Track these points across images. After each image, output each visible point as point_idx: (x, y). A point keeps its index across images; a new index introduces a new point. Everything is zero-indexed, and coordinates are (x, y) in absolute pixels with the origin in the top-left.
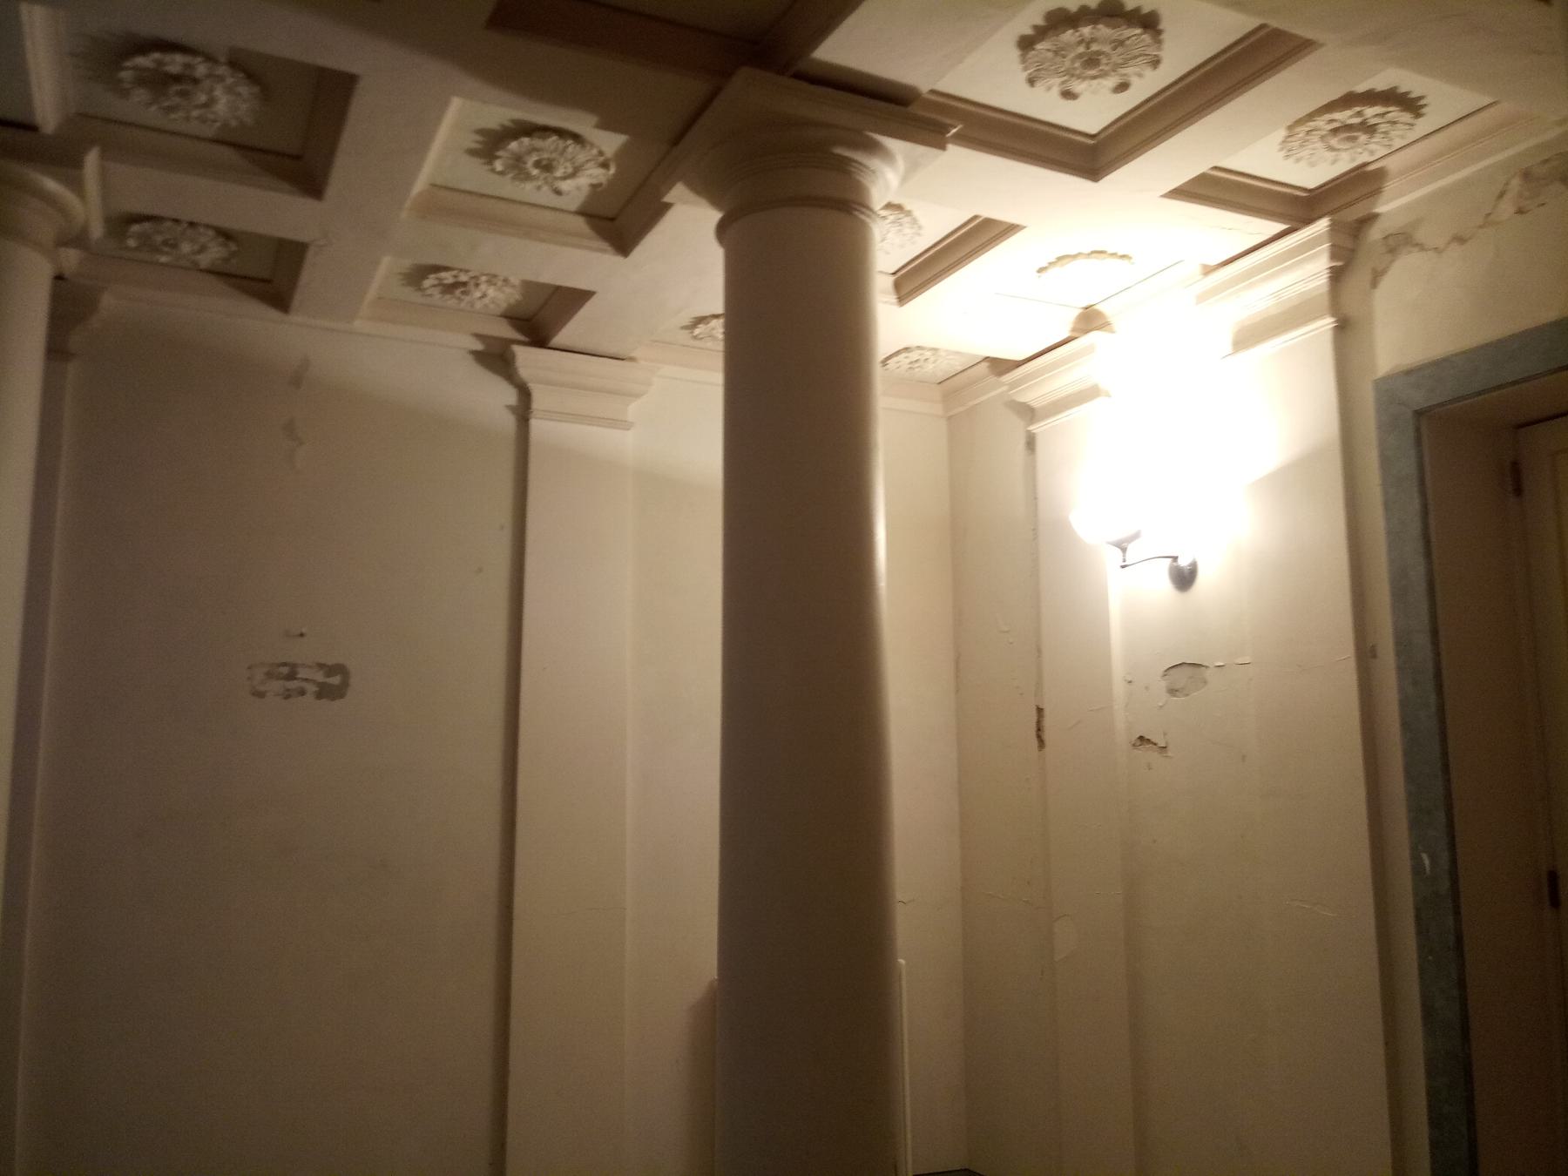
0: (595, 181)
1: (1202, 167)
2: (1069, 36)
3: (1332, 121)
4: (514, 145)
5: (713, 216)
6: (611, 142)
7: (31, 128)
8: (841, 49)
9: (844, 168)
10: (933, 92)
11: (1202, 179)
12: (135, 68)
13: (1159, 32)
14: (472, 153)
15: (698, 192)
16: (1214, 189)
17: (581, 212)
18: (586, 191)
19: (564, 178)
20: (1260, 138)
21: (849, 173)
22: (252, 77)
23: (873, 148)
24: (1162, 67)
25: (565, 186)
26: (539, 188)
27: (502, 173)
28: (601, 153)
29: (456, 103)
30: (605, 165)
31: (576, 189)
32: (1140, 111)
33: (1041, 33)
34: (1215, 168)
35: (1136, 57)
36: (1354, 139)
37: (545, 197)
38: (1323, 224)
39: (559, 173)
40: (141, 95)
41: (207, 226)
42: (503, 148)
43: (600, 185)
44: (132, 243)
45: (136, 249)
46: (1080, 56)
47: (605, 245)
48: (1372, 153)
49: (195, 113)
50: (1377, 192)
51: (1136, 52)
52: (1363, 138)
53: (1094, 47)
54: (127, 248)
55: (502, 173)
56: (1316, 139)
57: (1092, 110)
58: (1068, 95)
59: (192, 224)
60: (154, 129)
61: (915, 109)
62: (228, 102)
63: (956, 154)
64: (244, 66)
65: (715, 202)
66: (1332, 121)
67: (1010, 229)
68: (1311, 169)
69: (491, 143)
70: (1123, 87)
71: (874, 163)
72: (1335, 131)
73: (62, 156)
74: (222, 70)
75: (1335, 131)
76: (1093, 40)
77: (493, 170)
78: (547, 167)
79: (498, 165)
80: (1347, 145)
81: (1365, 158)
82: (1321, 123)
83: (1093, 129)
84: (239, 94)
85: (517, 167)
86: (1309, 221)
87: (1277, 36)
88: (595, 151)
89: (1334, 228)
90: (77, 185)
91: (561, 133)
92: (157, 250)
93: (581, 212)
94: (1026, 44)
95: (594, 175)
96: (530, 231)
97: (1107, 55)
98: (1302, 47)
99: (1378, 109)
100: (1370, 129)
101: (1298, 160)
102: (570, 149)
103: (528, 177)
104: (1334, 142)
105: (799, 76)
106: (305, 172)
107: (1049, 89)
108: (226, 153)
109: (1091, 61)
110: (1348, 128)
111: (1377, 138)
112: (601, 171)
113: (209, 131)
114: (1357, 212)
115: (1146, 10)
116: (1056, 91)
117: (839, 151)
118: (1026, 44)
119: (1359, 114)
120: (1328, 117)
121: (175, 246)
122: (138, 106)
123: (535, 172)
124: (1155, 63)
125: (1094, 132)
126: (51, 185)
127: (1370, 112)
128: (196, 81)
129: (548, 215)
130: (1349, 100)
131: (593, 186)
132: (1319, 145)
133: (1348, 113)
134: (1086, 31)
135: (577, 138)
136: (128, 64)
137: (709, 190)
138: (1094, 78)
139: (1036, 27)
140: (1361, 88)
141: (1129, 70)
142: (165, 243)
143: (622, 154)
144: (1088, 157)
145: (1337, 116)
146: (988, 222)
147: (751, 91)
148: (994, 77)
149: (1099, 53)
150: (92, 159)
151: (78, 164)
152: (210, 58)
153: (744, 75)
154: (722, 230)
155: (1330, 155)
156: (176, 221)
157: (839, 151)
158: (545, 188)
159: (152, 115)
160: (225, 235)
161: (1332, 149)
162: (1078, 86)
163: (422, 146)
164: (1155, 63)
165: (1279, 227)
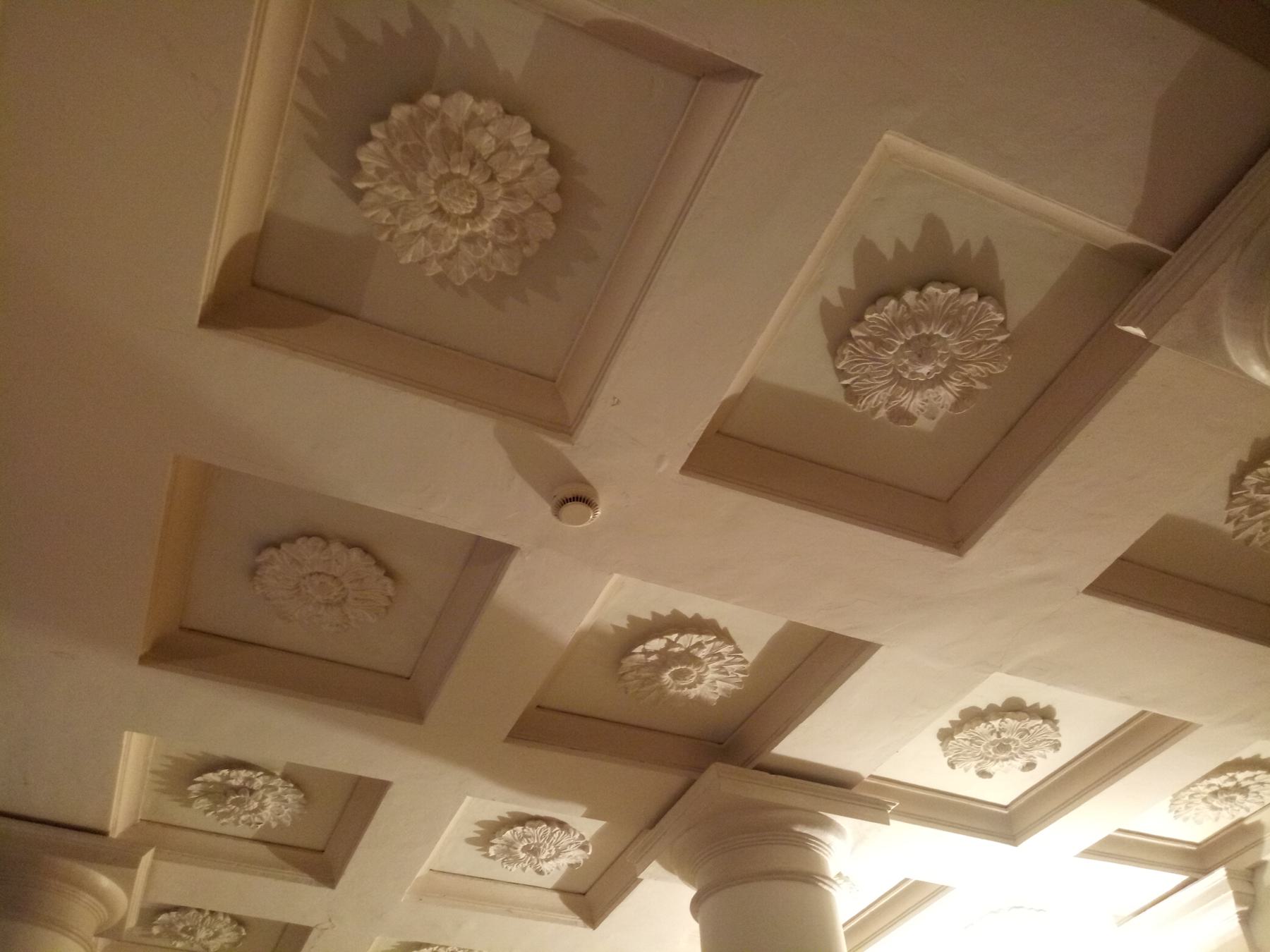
0: (573, 861)
1: (1109, 830)
2: (982, 728)
3: (1209, 786)
4: (508, 833)
5: (690, 892)
6: (590, 827)
7: (103, 833)
8: (799, 745)
9: (803, 842)
10: (872, 776)
11: (1109, 840)
12: (204, 782)
13: (1056, 722)
14: (470, 841)
15: (671, 871)
16: (1122, 848)
17: (555, 889)
18: (564, 869)
19: (547, 860)
20: (1160, 802)
21: (808, 848)
22: (298, 786)
23: (827, 825)
24: (1061, 749)
25: (545, 867)
26: (524, 869)
27: (494, 858)
28: (582, 837)
29: (468, 798)
30: (584, 847)
31: (555, 869)
32: (1045, 785)
33: (958, 726)
34: (1120, 830)
35: (1038, 743)
36: (1233, 799)
37: (529, 876)
38: (1220, 874)
39: (543, 857)
40: (204, 803)
41: (225, 915)
42: (500, 837)
43: (578, 864)
44: (156, 930)
45: (159, 936)
46: (992, 743)
47: (577, 918)
48: (1248, 810)
49: (243, 818)
50: (1259, 842)
51: (1039, 739)
52: (1239, 797)
53: (1004, 736)
54: (150, 936)
55: (494, 858)
56: (1200, 801)
57: (1005, 785)
58: (983, 774)
59: (212, 913)
60: (211, 833)
61: (856, 790)
62: (274, 807)
63: (898, 828)
64: (295, 778)
65: (689, 880)
66: (1209, 786)
67: (941, 890)
68: (1200, 825)
69: (488, 833)
70: (1030, 766)
71: (829, 838)
72: (1215, 794)
73: (122, 859)
74: (278, 782)
75: (1215, 794)
76: (1003, 730)
77: (487, 856)
78: (533, 851)
79: (492, 851)
80: (1228, 804)
81: (1243, 814)
82: (1201, 788)
83: (1005, 801)
84: (286, 801)
85: (508, 854)
86: (1206, 872)
87: (1157, 720)
88: (577, 836)
89: (1231, 875)
90: (128, 885)
91: (549, 821)
92: (178, 938)
93: (555, 889)
94: (945, 736)
95: (576, 855)
96: (510, 908)
97: (1015, 741)
98: (1180, 729)
99: (1248, 774)
100: (1244, 790)
101: (1186, 819)
102: (556, 835)
103: (517, 860)
104: (1215, 803)
105: (759, 768)
106: (321, 861)
107: (966, 770)
108: (263, 850)
109: (1003, 747)
110: (1226, 790)
111: (1251, 797)
112: (582, 852)
113: (249, 832)
114: (1247, 860)
115: (1042, 706)
116: (973, 771)
117: (798, 829)
118: (945, 736)
119: (1233, 778)
120: (1206, 782)
121: (193, 933)
122: (199, 814)
123: (523, 855)
124: (1056, 746)
125: (1006, 803)
126: (105, 882)
127: (1241, 776)
128: (252, 792)
129: (528, 893)
130: (1239, 765)
131: (571, 865)
132: (1203, 805)
133: (1223, 778)
134: (996, 723)
135: (562, 824)
136: (199, 779)
137: (683, 866)
138: (1006, 760)
139: (952, 722)
140: (1246, 754)
141: (1035, 753)
142: (185, 930)
143: (600, 835)
144: (1007, 824)
145: (1214, 781)
146: (918, 885)
147: (722, 782)
148: (920, 762)
149: (1009, 740)
150: (147, 859)
151: (134, 864)
152: (269, 773)
153: (715, 771)
154: (697, 905)
155: (1212, 814)
156: (199, 910)
157: (799, 829)
158: (529, 869)
159: (209, 821)
160: (239, 921)
161: (1214, 808)
162: (990, 767)
163: (433, 838)
164: (1056, 746)
165: (1182, 878)
